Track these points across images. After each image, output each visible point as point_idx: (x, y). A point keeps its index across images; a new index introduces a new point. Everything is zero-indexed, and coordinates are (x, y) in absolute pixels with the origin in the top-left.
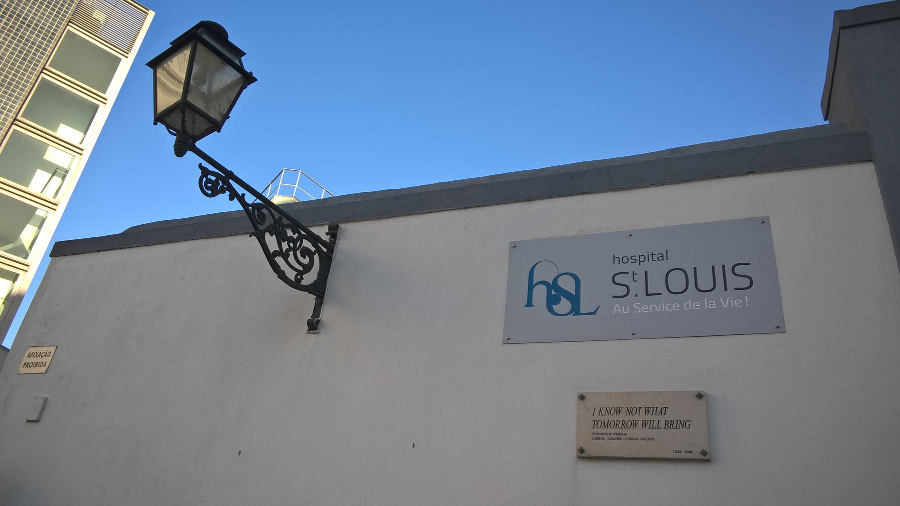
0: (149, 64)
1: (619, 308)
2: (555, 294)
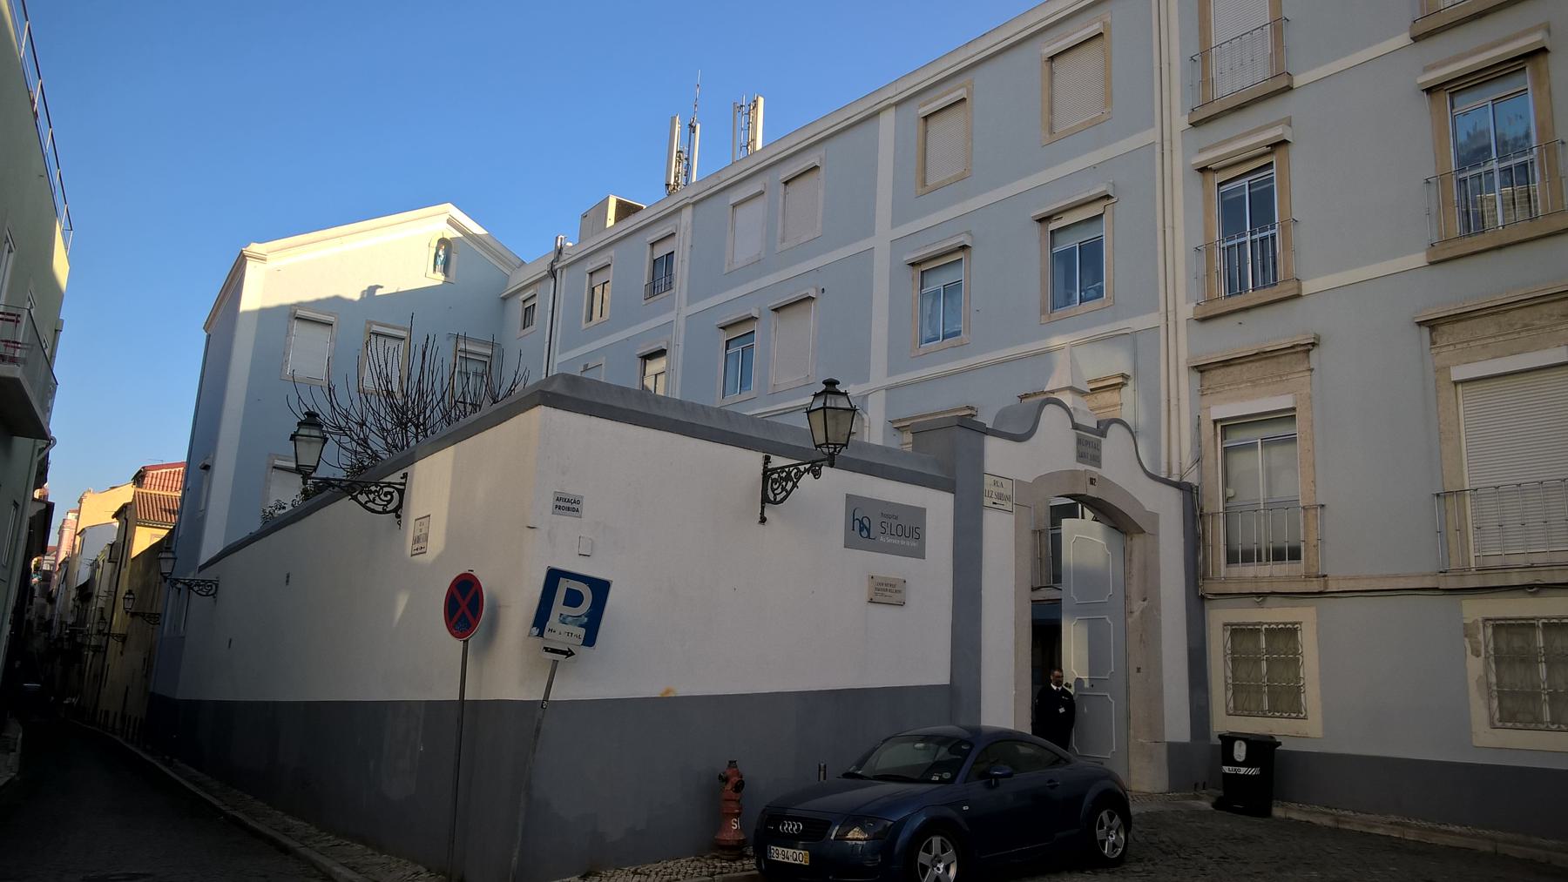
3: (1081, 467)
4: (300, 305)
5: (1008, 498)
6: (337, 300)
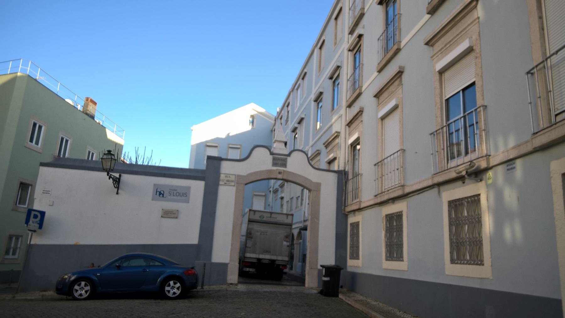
0: (375, 96)
1: (169, 197)
2: (160, 193)
3: (275, 168)
4: (207, 142)
5: (232, 181)
6: (218, 139)
